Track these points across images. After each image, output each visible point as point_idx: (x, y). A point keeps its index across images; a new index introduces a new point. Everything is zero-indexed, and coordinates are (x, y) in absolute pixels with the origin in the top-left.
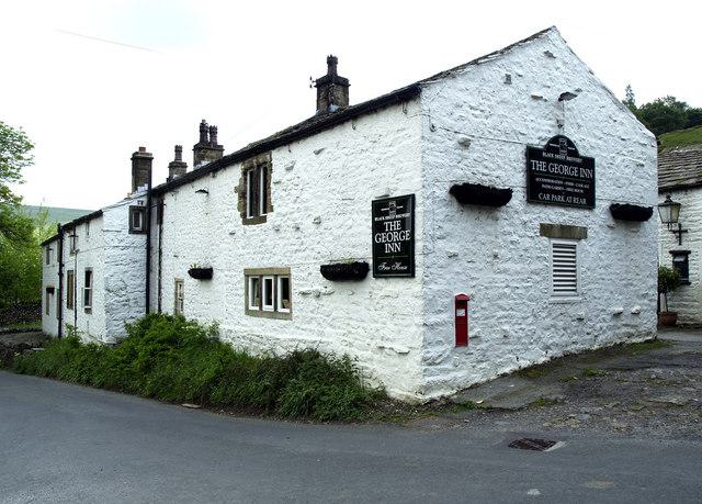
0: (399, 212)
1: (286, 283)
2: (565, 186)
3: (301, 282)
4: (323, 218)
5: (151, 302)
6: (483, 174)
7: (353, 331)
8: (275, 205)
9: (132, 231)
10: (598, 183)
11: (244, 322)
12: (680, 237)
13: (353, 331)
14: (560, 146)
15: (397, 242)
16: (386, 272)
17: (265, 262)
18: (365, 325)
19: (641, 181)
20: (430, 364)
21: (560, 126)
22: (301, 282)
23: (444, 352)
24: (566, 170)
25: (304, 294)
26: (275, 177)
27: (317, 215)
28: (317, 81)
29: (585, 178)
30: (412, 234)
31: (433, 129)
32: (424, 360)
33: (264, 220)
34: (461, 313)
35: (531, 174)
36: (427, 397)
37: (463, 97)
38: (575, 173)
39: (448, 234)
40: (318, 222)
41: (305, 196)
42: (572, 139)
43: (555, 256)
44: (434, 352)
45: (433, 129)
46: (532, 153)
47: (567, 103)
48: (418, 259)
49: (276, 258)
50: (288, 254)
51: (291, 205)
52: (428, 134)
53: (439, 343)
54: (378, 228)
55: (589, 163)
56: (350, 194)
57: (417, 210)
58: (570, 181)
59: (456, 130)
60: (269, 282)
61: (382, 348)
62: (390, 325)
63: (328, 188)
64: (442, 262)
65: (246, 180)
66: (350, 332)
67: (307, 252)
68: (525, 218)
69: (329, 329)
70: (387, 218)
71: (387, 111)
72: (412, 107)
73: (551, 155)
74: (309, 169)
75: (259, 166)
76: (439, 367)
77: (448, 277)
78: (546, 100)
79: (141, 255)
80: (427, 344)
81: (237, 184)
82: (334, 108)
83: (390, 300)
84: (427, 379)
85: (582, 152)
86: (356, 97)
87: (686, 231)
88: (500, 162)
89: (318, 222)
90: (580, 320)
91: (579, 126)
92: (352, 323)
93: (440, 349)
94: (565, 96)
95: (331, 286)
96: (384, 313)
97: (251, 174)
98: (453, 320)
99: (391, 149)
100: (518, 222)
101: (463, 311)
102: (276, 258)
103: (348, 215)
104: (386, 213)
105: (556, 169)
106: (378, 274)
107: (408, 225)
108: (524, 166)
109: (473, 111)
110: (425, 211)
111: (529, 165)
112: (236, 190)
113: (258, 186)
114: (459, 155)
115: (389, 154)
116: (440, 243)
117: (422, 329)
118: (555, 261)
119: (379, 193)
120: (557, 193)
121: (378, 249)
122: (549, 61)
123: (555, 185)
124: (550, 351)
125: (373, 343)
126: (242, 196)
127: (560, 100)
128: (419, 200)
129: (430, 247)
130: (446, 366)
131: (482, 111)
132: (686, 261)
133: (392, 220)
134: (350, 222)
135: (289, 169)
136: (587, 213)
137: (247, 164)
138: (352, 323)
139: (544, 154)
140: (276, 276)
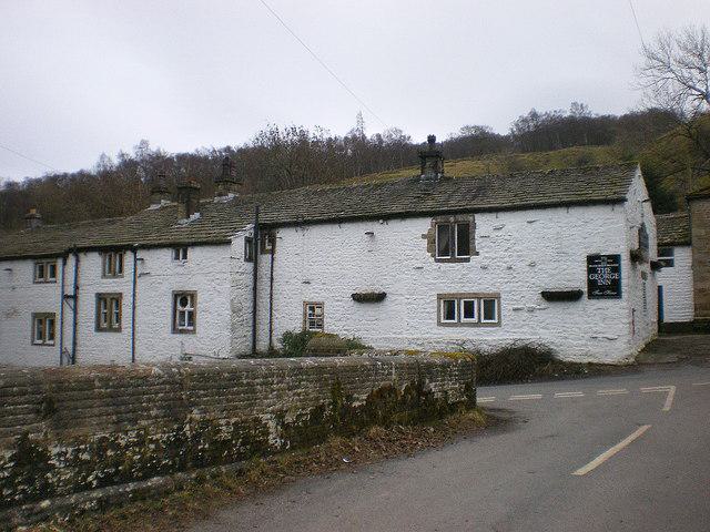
5: (259, 332)
9: (246, 260)
11: (435, 331)
54: (591, 271)
79: (249, 280)
95: (545, 304)
104: (599, 263)
106: (591, 296)
119: (593, 251)
121: (592, 284)
122: (534, 225)
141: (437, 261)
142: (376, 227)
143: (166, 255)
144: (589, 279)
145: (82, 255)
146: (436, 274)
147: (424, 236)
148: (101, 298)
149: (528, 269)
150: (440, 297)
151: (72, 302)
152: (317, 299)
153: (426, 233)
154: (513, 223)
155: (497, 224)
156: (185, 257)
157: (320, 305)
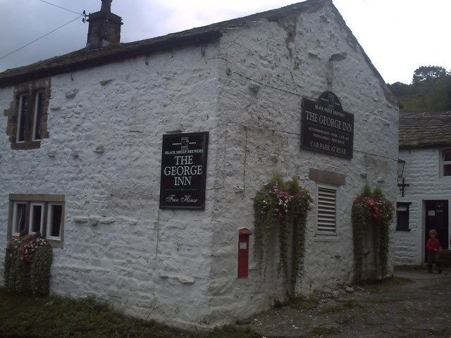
0: (191, 147)
1: (58, 212)
2: (331, 137)
3: (77, 211)
4: (106, 148)
6: (267, 120)
7: (134, 261)
8: (51, 132)
10: (356, 137)
12: (403, 190)
13: (134, 261)
14: (329, 99)
15: (187, 176)
16: (172, 204)
17: (35, 188)
18: (147, 255)
19: (387, 138)
20: (215, 295)
21: (329, 84)
22: (77, 211)
23: (227, 283)
24: (332, 122)
25: (79, 222)
26: (53, 103)
27: (98, 144)
28: (90, 15)
29: (346, 132)
30: (204, 170)
31: (229, 73)
32: (210, 290)
33: (37, 145)
34: (244, 246)
35: (305, 123)
36: (212, 326)
37: (255, 47)
38: (339, 127)
39: (236, 172)
40: (100, 152)
41: (86, 125)
42: (338, 96)
43: (319, 199)
44: (219, 282)
45: (229, 73)
46: (307, 105)
47: (337, 64)
48: (209, 193)
49: (49, 185)
50: (63, 182)
51: (71, 133)
52: (224, 77)
53: (223, 274)
54: (167, 161)
55: (349, 118)
56: (139, 126)
57: (211, 146)
58: (343, 135)
59: (248, 75)
60: (37, 210)
61: (165, 278)
62: (175, 256)
63: (114, 119)
64: (229, 197)
65: (18, 103)
66: (130, 262)
67: (86, 180)
68: (298, 162)
69: (105, 259)
70: (179, 152)
71: (118, 64)
72: (211, 51)
73: (321, 108)
74: (93, 98)
75: (35, 91)
76: (222, 297)
77: (234, 211)
78: (319, 59)
80: (214, 274)
81: (8, 107)
82: (105, 43)
83: (176, 231)
84: (212, 309)
85: (345, 108)
86: (130, 34)
87: (408, 185)
88: (281, 110)
89: (100, 152)
90: (338, 257)
91: (344, 85)
92: (132, 253)
93: (224, 280)
94: (335, 57)
96: (170, 243)
97: (24, 98)
98: (236, 252)
99: (186, 87)
100: (292, 165)
101: (245, 244)
102: (49, 185)
103: (135, 147)
104: (178, 148)
105: (324, 121)
107: (201, 160)
108: (299, 115)
109: (262, 61)
110: (219, 149)
111: (304, 115)
112: (6, 113)
113: (31, 113)
114: (248, 99)
115: (183, 92)
116: (229, 180)
117: (210, 260)
118: (319, 203)
119: (172, 128)
120: (324, 142)
123: (324, 135)
124: (313, 286)
125: (155, 274)
126: (13, 120)
127: (331, 60)
128: (213, 138)
129: (221, 182)
130: (229, 296)
131: (269, 62)
132: (408, 211)
133: (184, 156)
134: (137, 154)
135: (70, 97)
136: (346, 162)
137: (21, 88)
138: (132, 253)
139: (316, 107)
140: (47, 203)
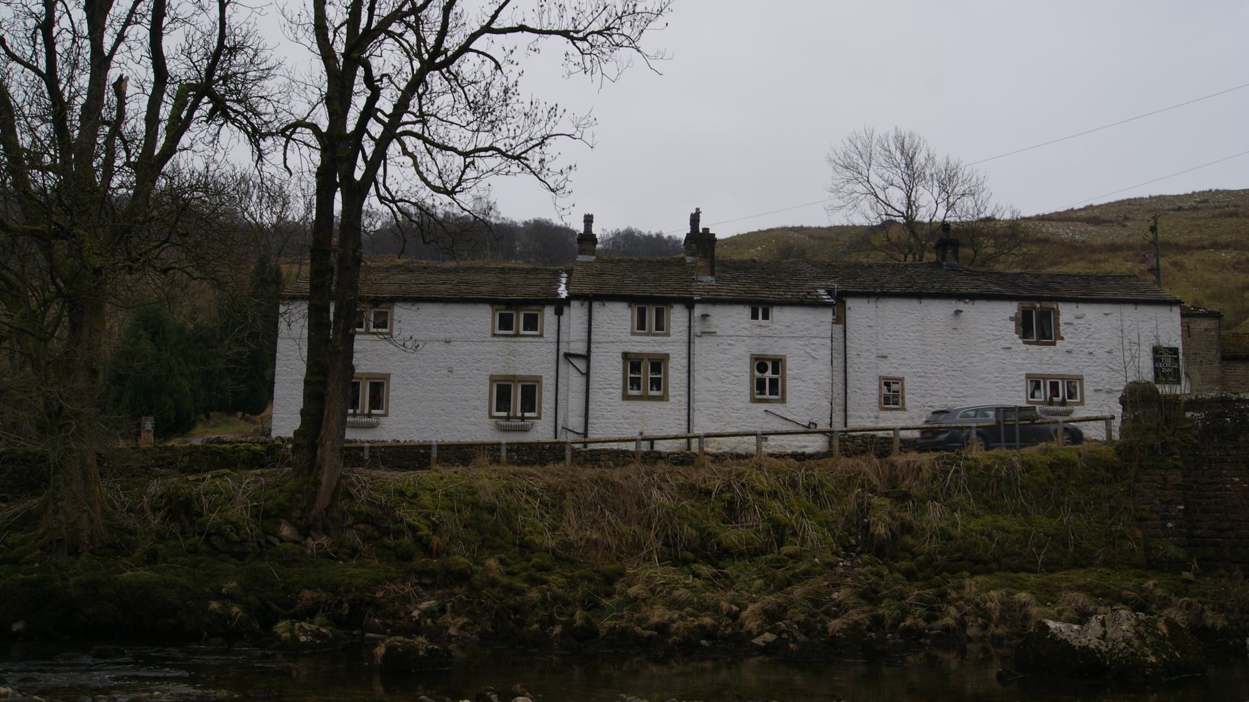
54: (1156, 360)
122: (1110, 317)
141: (1025, 343)
142: (961, 305)
143: (741, 314)
144: (1155, 368)
145: (596, 305)
146: (1023, 356)
147: (1011, 319)
148: (632, 362)
149: (1106, 354)
150: (1028, 376)
151: (581, 365)
152: (896, 374)
153: (1013, 315)
154: (1091, 312)
155: (1079, 313)
156: (766, 317)
157: (900, 380)
